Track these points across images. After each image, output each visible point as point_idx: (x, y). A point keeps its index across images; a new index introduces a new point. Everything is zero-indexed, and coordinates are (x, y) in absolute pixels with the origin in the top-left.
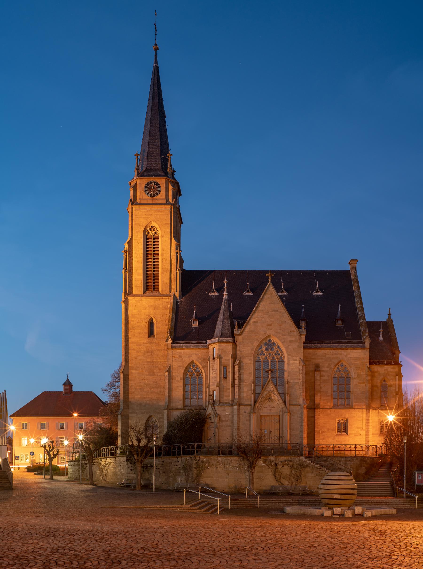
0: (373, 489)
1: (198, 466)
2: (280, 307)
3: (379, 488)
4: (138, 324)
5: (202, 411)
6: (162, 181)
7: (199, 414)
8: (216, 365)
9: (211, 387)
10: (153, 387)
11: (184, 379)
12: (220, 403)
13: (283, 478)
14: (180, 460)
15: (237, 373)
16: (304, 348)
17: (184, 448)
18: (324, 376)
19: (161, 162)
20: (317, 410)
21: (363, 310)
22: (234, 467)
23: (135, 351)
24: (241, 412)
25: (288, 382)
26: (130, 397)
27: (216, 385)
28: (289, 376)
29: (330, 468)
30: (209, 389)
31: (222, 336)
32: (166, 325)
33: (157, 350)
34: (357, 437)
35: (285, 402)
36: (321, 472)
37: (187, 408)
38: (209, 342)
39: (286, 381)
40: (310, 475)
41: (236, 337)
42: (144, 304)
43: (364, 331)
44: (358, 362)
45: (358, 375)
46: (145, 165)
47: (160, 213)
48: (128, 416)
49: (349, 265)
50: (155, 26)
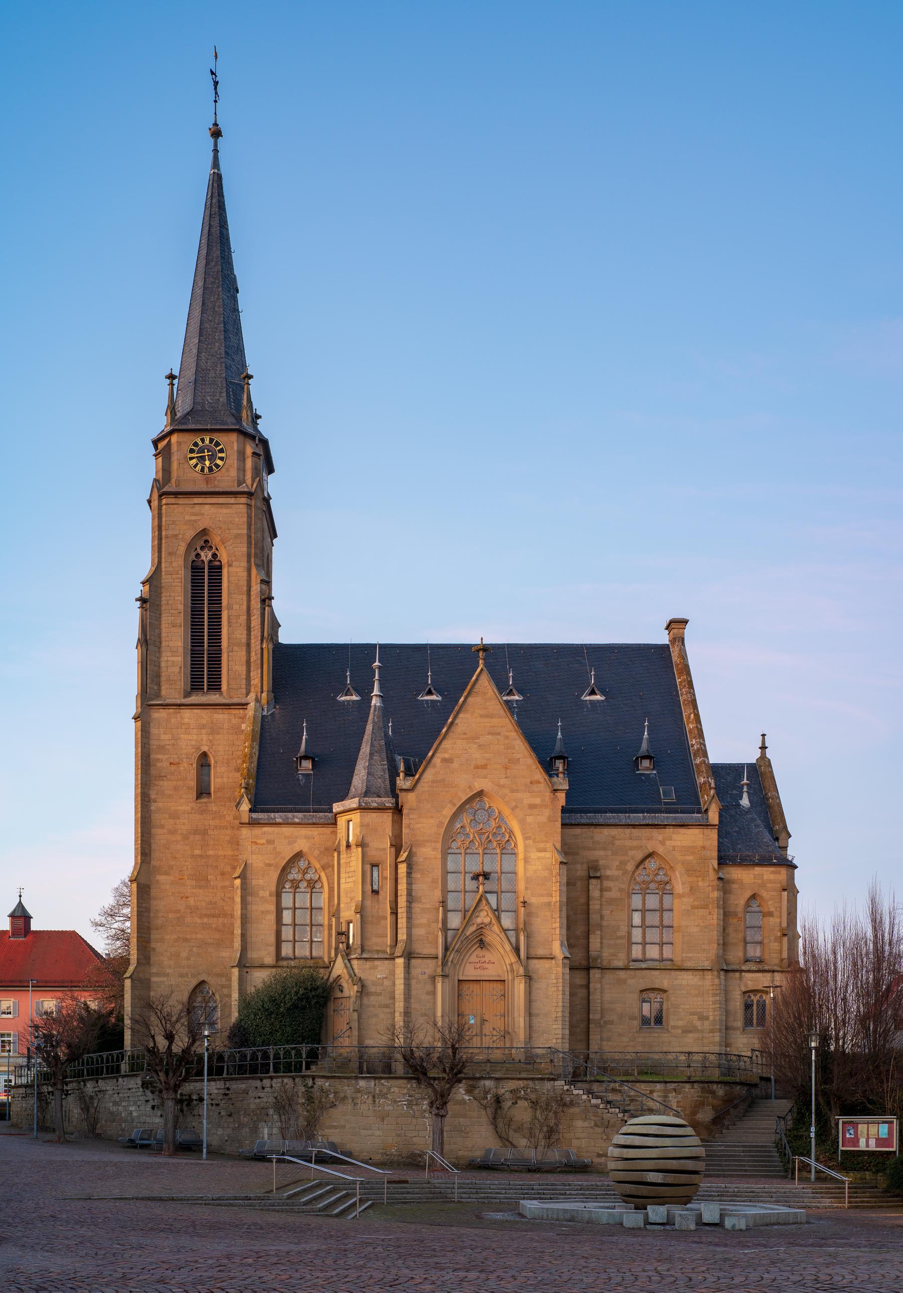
0: (734, 1161)
1: (310, 1099)
2: (506, 725)
3: (749, 1156)
4: (173, 768)
5: (321, 970)
6: (230, 442)
7: (313, 979)
8: (353, 862)
10: (205, 915)
12: (363, 951)
13: (515, 1131)
14: (268, 1085)
15: (405, 880)
16: (563, 825)
17: (277, 1056)
18: (609, 889)
19: (228, 393)
20: (595, 974)
21: (700, 734)
22: (396, 1102)
23: (166, 831)
24: (414, 972)
25: (525, 902)
26: (152, 937)
27: (353, 908)
28: (526, 888)
29: (627, 1108)
30: (338, 919)
31: (367, 794)
32: (238, 770)
33: (216, 827)
34: (690, 1035)
35: (517, 950)
36: (607, 1116)
37: (285, 963)
38: (337, 807)
39: (521, 899)
40: (579, 1123)
41: (402, 795)
42: (186, 720)
43: (705, 783)
45: (691, 888)
46: (189, 400)
47: (225, 511)
48: (149, 980)
49: (667, 632)
50: (216, 93)
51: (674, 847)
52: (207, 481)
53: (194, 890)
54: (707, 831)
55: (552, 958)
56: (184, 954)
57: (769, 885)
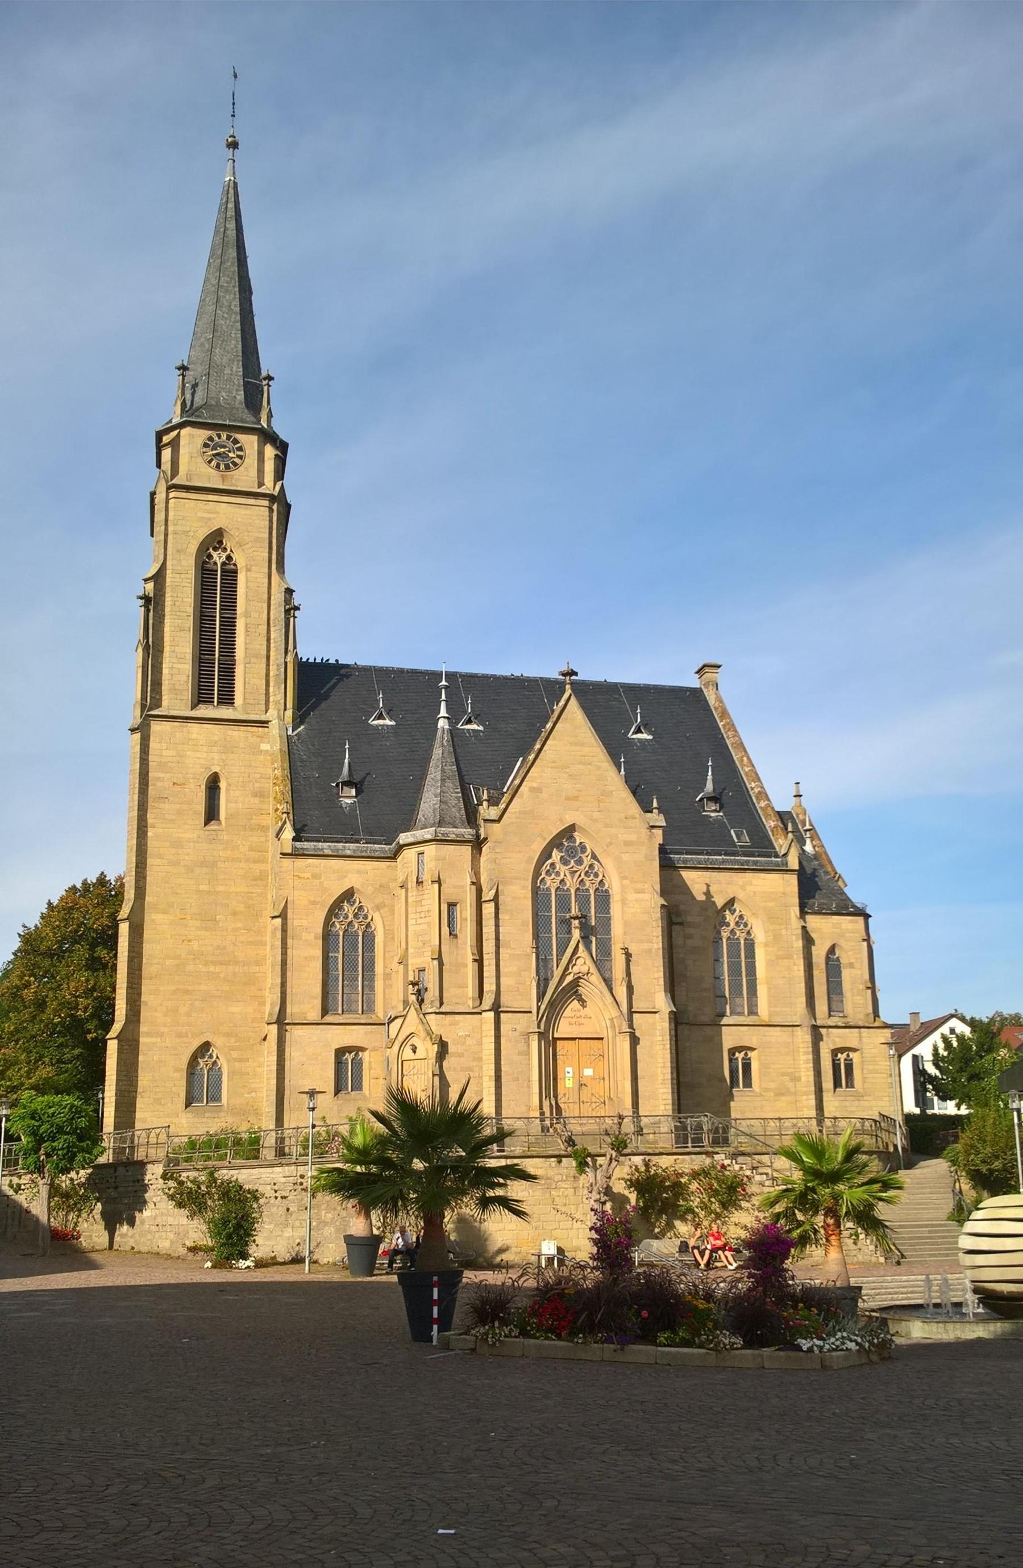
4: (177, 788)
9: (410, 962)
10: (212, 962)
11: (328, 936)
18: (690, 937)
34: (783, 1098)
38: (404, 838)
42: (194, 736)
44: (771, 904)
45: (775, 936)
51: (755, 893)
52: (223, 478)
53: (199, 933)
54: (787, 876)
55: (655, 1013)
56: (183, 1010)
57: (848, 935)
